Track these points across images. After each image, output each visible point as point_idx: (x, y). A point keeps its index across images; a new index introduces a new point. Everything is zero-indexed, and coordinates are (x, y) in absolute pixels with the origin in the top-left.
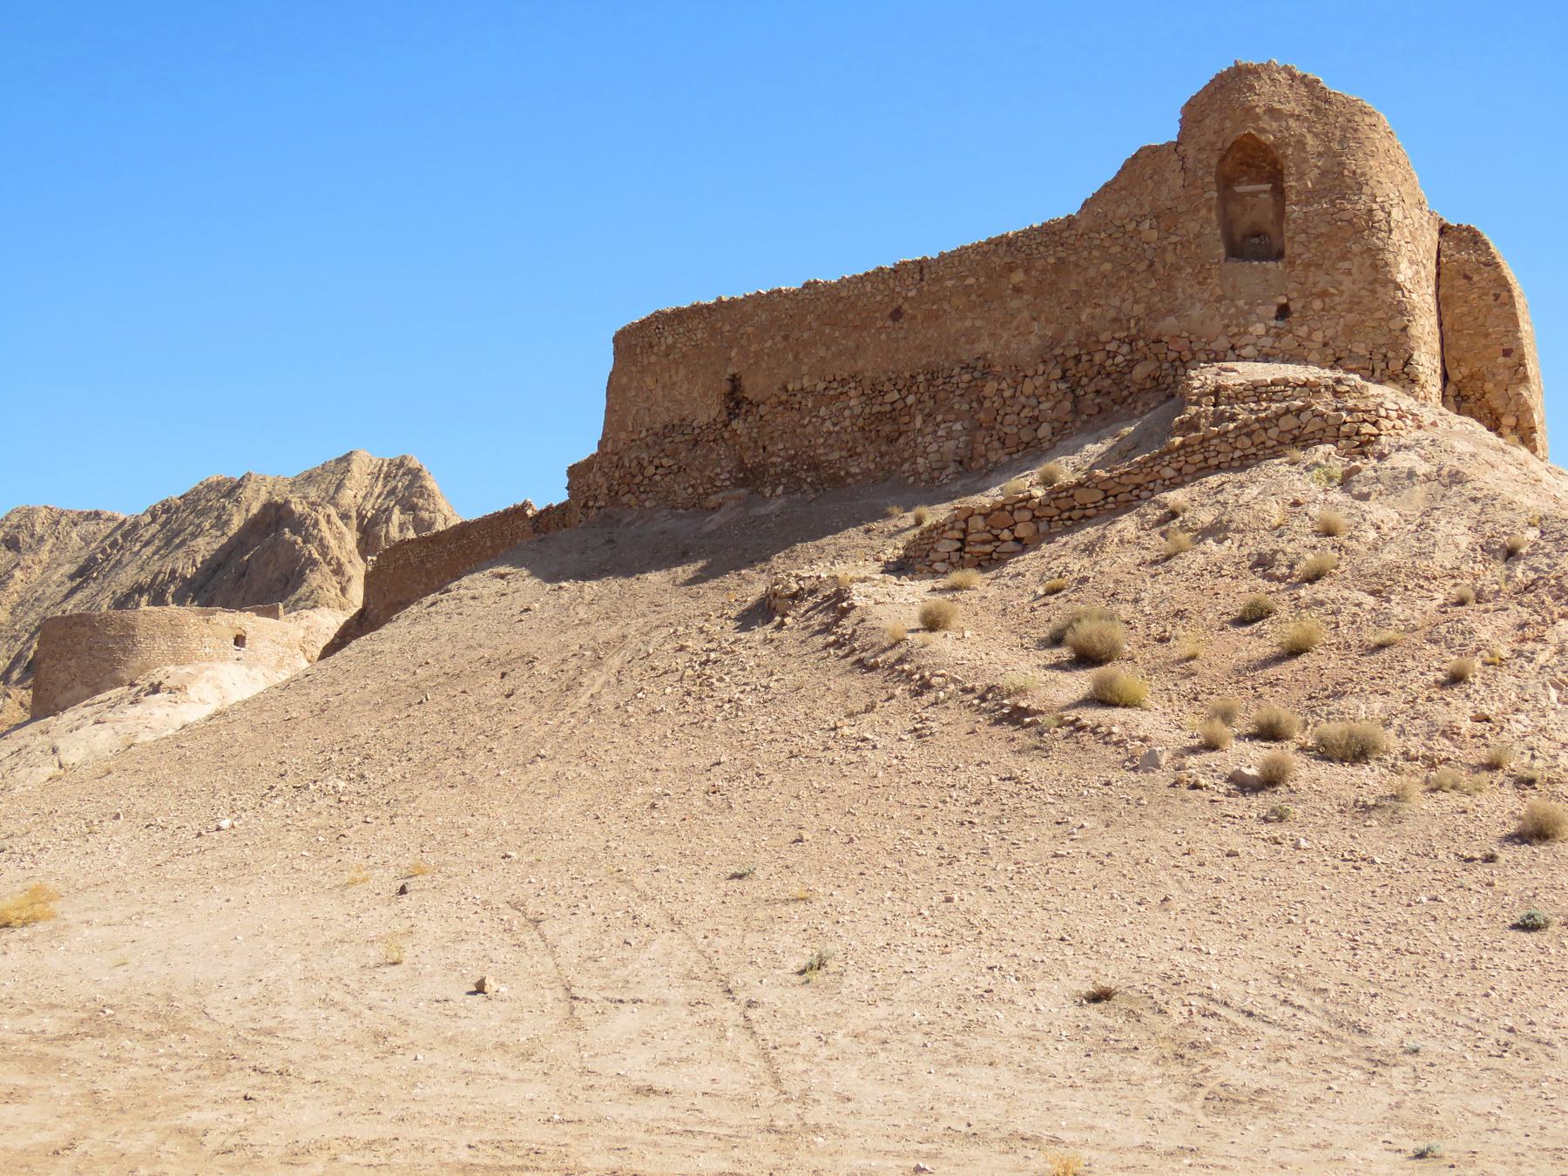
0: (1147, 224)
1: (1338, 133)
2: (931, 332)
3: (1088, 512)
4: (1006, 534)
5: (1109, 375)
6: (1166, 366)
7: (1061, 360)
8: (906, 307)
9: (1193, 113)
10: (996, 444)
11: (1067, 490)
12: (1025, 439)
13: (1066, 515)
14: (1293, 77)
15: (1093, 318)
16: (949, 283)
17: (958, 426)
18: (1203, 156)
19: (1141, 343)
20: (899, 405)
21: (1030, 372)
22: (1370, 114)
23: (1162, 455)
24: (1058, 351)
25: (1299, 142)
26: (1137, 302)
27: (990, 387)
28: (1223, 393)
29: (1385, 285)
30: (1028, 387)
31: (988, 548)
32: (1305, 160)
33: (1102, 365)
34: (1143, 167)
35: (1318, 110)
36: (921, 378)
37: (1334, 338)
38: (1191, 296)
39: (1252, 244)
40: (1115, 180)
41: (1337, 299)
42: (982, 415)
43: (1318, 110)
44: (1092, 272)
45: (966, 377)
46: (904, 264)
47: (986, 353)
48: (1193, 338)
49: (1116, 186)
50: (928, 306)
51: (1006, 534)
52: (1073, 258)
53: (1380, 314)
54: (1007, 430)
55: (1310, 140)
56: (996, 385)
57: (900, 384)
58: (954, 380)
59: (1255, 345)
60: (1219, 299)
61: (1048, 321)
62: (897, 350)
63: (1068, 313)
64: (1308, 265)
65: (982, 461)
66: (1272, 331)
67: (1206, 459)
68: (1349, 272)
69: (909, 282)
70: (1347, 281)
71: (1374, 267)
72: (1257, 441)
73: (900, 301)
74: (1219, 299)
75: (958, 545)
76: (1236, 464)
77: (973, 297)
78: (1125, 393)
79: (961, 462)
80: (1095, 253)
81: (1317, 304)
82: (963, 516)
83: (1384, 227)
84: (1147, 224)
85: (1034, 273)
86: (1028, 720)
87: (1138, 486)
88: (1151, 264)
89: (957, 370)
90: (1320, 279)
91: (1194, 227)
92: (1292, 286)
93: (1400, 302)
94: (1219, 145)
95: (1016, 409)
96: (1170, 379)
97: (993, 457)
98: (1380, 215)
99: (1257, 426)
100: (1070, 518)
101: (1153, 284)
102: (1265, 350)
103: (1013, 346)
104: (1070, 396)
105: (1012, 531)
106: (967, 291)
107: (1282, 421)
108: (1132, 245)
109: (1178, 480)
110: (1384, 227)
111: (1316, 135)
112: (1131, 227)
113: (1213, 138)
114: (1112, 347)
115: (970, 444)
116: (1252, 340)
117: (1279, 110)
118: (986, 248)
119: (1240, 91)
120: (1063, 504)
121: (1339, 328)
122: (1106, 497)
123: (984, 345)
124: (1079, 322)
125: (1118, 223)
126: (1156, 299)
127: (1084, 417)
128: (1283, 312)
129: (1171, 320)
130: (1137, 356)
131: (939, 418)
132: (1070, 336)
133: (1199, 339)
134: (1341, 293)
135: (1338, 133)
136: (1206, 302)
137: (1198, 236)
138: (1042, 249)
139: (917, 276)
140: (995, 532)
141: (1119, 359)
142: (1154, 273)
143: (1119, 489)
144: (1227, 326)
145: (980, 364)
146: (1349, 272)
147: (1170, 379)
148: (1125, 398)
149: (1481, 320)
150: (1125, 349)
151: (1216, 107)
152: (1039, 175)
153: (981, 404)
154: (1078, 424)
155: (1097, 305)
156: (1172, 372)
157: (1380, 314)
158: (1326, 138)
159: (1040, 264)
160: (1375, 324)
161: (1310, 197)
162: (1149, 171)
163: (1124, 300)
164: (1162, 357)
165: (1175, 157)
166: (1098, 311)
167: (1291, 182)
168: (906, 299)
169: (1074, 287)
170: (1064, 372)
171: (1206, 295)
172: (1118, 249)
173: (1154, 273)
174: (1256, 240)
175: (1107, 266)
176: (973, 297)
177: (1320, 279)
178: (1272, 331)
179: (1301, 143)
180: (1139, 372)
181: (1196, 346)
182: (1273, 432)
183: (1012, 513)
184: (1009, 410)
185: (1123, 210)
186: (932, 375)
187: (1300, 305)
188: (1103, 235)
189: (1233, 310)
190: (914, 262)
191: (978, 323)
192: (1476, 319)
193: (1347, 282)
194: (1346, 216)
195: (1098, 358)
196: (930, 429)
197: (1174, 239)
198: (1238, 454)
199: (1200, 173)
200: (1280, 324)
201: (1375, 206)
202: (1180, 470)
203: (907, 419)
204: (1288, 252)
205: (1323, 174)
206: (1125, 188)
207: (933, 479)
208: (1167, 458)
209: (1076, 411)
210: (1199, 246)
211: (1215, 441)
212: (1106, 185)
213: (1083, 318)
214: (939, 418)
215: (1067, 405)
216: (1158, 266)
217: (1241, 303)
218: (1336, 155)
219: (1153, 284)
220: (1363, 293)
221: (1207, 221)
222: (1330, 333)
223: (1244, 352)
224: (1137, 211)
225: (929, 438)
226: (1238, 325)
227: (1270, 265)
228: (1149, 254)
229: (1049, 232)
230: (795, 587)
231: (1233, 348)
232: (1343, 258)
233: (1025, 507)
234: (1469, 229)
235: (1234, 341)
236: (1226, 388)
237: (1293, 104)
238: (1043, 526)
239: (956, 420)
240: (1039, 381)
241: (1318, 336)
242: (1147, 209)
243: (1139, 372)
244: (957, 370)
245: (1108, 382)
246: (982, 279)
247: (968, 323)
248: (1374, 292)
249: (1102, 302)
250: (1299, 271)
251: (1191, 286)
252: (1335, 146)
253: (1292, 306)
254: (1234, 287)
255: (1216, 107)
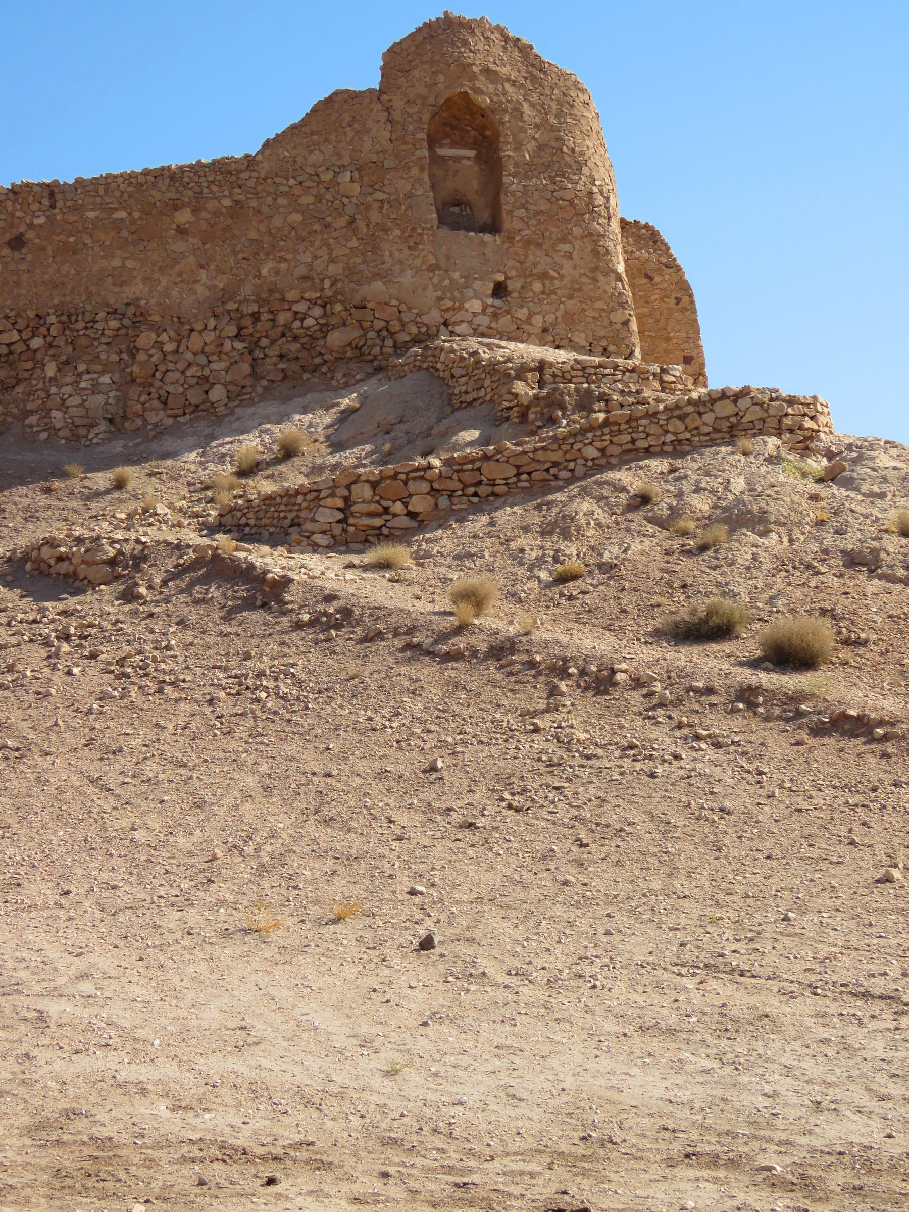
0: (347, 176)
1: (554, 106)
2: (65, 268)
3: (497, 489)
4: (398, 507)
5: (296, 338)
6: (372, 334)
7: (237, 317)
8: (30, 235)
9: (398, 60)
10: (156, 403)
11: (473, 461)
12: (194, 401)
13: (471, 490)
14: (506, 39)
15: (277, 273)
16: (92, 215)
17: (105, 379)
18: (413, 110)
19: (338, 307)
20: (20, 348)
21: (198, 326)
22: (584, 91)
23: (583, 431)
24: (232, 306)
25: (516, 109)
26: (333, 260)
27: (146, 339)
28: (548, 371)
29: (606, 275)
30: (196, 342)
31: (377, 522)
32: (523, 130)
33: (288, 327)
34: (336, 110)
35: (533, 79)
36: (52, 319)
37: (555, 324)
38: (400, 262)
39: (472, 213)
40: (305, 122)
41: (557, 283)
42: (136, 369)
43: (533, 79)
44: (277, 222)
45: (114, 324)
46: (28, 185)
47: (138, 299)
48: (403, 307)
49: (306, 130)
50: (63, 237)
51: (398, 507)
52: (254, 203)
53: (600, 305)
54: (171, 389)
55: (526, 107)
56: (154, 336)
57: (21, 324)
58: (99, 326)
59: (470, 322)
60: (432, 268)
61: (220, 271)
62: (17, 284)
63: (245, 264)
64: (527, 243)
65: (139, 422)
66: (489, 310)
67: (633, 441)
68: (570, 256)
69: (35, 206)
70: (567, 266)
71: (595, 253)
72: (691, 426)
73: (23, 228)
74: (432, 268)
75: (340, 516)
76: (669, 449)
77: (125, 233)
78: (318, 360)
79: (111, 421)
80: (282, 201)
81: (537, 286)
82: (345, 482)
83: (604, 213)
84: (347, 176)
85: (204, 214)
86: (880, 731)
87: (555, 464)
88: (352, 221)
89: (101, 315)
90: (539, 259)
91: (404, 186)
92: (511, 263)
93: (620, 294)
94: (431, 100)
95: (181, 366)
96: (377, 350)
97: (153, 418)
98: (600, 200)
99: (690, 409)
100: (476, 495)
101: (354, 243)
102: (481, 329)
103: (175, 294)
104: (249, 358)
105: (406, 505)
106: (117, 226)
107: (718, 406)
108: (329, 196)
109: (603, 461)
110: (604, 213)
111: (532, 105)
112: (327, 176)
113: (425, 92)
114: (301, 307)
115: (123, 400)
116: (468, 317)
117: (495, 72)
118: (141, 179)
119: (453, 44)
120: (468, 477)
121: (559, 314)
122: (518, 475)
123: (135, 290)
124: (259, 276)
125: (310, 170)
126: (358, 260)
127: (265, 383)
128: (500, 290)
129: (378, 285)
130: (333, 321)
131: (82, 367)
132: (247, 290)
133: (410, 309)
134: (562, 277)
135: (554, 106)
136: (418, 270)
137: (409, 196)
138: (214, 188)
139: (46, 202)
140: (385, 503)
141: (309, 322)
142: (355, 231)
143: (534, 465)
144: (440, 299)
145: (131, 310)
146: (570, 256)
147: (377, 350)
148: (317, 366)
149: (661, 324)
150: (317, 311)
151: (426, 58)
152: (225, 109)
153: (133, 356)
154: (260, 390)
155: (282, 259)
156: (378, 341)
157: (600, 305)
158: (543, 109)
159: (211, 205)
160: (596, 314)
161: (528, 170)
162: (347, 118)
163: (315, 257)
164: (366, 324)
165: (379, 106)
166: (283, 266)
167: (508, 151)
168: (31, 226)
169: (253, 235)
170: (240, 329)
171: (418, 262)
172: (311, 199)
173: (355, 231)
174: (456, 209)
175: (296, 217)
176: (125, 233)
177: (543, 263)
178: (489, 310)
179: (518, 112)
180: (336, 339)
181: (406, 317)
182: (709, 418)
183: (405, 483)
184: (171, 366)
185: (316, 157)
186: (68, 318)
187: (518, 285)
188: (292, 182)
189: (447, 282)
190: (42, 185)
191: (130, 264)
192: (658, 321)
193: (567, 266)
194: (568, 195)
195: (282, 318)
196: (69, 379)
197: (380, 196)
198: (669, 438)
199: (411, 128)
200: (498, 303)
201: (595, 190)
202: (603, 450)
203: (29, 365)
204: (507, 225)
205: (541, 147)
206: (318, 133)
207: (77, 438)
208: (590, 435)
209: (255, 375)
210: (409, 207)
211: (644, 422)
212: (293, 127)
213: (264, 272)
214: (82, 367)
215: (246, 367)
216: (361, 224)
217: (456, 275)
218: (553, 129)
219: (354, 243)
220: (584, 279)
221: (419, 181)
222: (550, 318)
223: (458, 329)
224: (334, 159)
225: (68, 389)
226: (453, 299)
227: (487, 237)
228: (350, 209)
229: (223, 170)
230: (111, 552)
231: (446, 324)
232: (563, 240)
233: (422, 478)
234: (647, 226)
235: (447, 315)
236: (551, 365)
237: (508, 67)
238: (443, 502)
239: (103, 372)
240: (209, 337)
241: (538, 320)
242: (346, 160)
243: (336, 339)
244: (101, 315)
245: (295, 347)
246: (136, 215)
247: (116, 263)
248: (595, 280)
249: (289, 256)
250: (518, 248)
251: (400, 250)
252: (553, 120)
253: (510, 285)
254: (448, 257)
255: (426, 58)
